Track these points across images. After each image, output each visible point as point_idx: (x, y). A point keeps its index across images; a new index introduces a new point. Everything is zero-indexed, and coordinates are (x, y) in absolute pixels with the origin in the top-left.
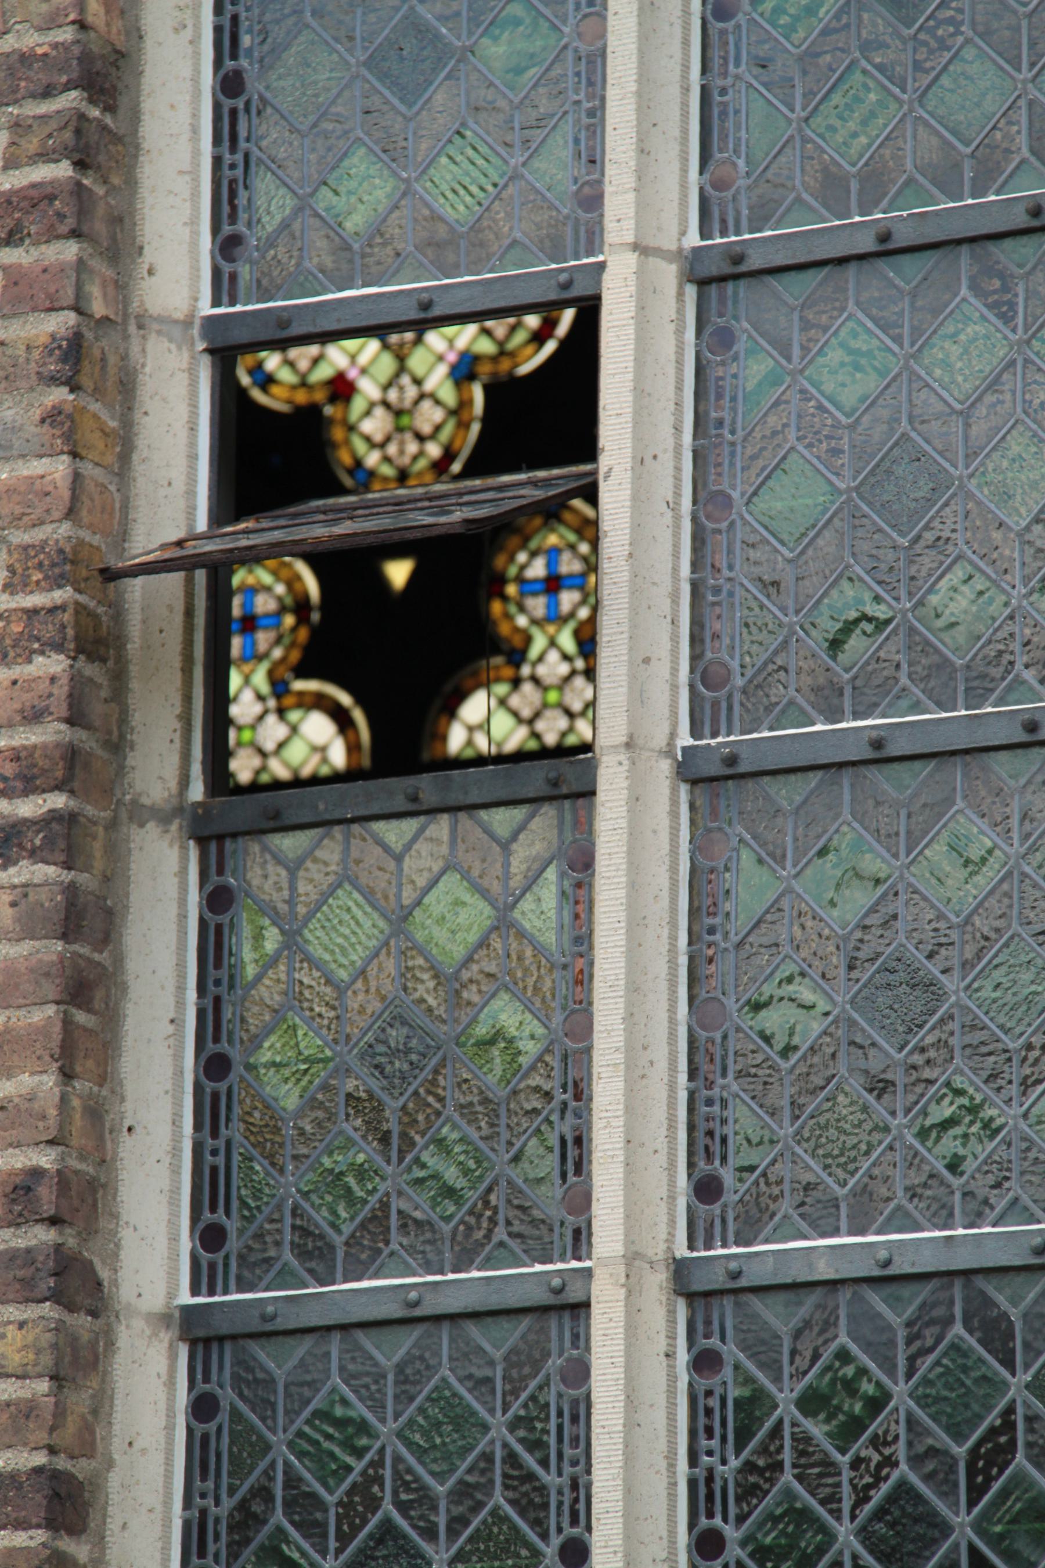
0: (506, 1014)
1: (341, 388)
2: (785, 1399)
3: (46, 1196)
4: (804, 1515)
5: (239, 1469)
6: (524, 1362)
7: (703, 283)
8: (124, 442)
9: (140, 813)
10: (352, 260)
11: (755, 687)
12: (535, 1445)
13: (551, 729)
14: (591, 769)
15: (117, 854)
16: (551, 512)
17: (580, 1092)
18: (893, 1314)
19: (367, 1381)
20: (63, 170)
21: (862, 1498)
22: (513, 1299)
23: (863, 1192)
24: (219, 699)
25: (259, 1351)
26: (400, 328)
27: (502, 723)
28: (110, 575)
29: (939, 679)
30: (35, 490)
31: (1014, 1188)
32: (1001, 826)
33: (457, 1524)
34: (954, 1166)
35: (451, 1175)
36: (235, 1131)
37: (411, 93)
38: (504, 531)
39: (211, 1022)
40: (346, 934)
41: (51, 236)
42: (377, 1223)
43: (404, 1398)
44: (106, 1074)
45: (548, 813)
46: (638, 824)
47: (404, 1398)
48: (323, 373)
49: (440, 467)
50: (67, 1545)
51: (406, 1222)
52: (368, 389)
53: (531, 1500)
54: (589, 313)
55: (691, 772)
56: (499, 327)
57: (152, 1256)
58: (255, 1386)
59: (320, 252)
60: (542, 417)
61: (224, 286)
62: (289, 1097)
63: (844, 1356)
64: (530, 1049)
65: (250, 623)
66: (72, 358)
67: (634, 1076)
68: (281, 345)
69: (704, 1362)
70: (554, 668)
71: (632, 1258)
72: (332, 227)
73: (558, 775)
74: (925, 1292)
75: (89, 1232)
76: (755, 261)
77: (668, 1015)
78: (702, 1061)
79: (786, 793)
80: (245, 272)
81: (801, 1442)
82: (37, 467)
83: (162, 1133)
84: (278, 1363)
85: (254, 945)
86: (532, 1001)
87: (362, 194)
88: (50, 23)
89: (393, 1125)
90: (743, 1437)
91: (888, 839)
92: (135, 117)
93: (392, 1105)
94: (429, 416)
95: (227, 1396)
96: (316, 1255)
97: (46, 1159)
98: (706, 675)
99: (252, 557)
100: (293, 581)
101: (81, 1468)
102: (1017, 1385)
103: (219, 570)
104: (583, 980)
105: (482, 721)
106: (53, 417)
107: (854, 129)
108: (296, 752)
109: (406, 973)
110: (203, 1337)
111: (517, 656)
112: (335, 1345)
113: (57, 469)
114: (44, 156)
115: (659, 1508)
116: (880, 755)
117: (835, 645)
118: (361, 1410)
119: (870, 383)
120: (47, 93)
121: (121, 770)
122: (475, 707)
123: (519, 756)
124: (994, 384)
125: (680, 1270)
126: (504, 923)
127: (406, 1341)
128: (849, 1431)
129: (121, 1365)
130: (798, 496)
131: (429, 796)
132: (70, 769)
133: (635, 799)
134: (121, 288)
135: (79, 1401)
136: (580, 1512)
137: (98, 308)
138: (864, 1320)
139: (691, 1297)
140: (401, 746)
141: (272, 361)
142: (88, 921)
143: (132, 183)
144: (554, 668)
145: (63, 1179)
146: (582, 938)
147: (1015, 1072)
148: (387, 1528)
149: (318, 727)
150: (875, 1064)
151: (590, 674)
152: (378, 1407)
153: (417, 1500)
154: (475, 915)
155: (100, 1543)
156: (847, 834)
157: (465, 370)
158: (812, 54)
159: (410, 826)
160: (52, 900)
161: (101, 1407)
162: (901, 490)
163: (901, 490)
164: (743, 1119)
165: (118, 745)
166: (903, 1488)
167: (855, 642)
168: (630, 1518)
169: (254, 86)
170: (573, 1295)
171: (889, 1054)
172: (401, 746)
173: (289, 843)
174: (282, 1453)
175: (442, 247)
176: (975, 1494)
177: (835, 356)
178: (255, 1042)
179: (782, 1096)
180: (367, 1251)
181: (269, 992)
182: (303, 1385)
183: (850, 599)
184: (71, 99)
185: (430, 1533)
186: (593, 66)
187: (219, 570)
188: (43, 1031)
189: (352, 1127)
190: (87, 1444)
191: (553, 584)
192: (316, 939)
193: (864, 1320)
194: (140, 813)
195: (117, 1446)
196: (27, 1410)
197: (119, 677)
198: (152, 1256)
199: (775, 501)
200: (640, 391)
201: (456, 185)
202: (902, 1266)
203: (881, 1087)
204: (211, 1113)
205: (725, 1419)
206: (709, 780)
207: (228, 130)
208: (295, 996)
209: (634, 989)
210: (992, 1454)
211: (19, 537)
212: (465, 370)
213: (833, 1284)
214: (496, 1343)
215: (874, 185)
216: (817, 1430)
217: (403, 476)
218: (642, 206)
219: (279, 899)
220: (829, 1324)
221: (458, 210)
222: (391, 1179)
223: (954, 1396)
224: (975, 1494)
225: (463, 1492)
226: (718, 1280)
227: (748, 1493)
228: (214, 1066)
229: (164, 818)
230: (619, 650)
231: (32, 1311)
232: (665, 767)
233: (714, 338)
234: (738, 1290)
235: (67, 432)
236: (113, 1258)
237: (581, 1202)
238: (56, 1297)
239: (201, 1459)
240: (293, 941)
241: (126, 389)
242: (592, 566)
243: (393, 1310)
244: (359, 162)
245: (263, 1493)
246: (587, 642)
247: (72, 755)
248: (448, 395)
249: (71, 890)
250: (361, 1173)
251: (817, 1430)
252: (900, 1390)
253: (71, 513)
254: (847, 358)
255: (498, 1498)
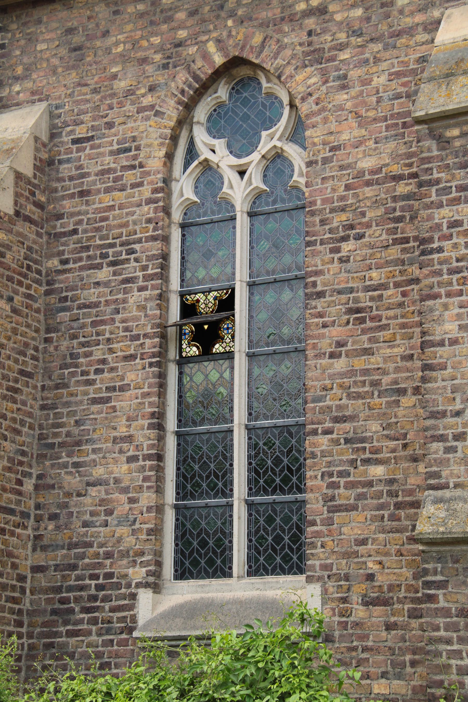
0: (222, 390)
1: (198, 301)
2: (261, 443)
3: (157, 415)
4: (263, 460)
5: (184, 453)
6: (224, 438)
7: (250, 286)
8: (167, 308)
9: (170, 361)
10: (200, 282)
11: (257, 343)
12: (226, 450)
13: (228, 349)
14: (234, 354)
15: (166, 366)
16: (228, 318)
17: (232, 400)
18: (276, 432)
19: (202, 441)
20: (159, 270)
21: (272, 457)
22: (223, 430)
23: (272, 414)
24: (181, 345)
25: (187, 437)
26: (206, 292)
27: (221, 348)
28: (166, 327)
29: (283, 342)
30: (155, 315)
31: (293, 414)
32: (292, 363)
33: (215, 461)
34: (285, 411)
35: (214, 412)
36: (183, 406)
37: (208, 259)
38: (221, 321)
39: (180, 390)
40: (199, 378)
41: (158, 279)
42: (203, 419)
43: (207, 443)
44: (165, 398)
45: (228, 361)
46: (241, 362)
47: (207, 443)
48: (195, 299)
49: (212, 312)
50: (160, 463)
51: (207, 419)
52: (202, 301)
53: (225, 458)
54: (233, 290)
55: (248, 355)
56: (220, 292)
57: (171, 423)
58: (186, 442)
59: (195, 281)
60: (227, 304)
61: (182, 286)
62: (191, 401)
63: (269, 437)
64: (225, 394)
65: (185, 334)
66: (160, 297)
67: (240, 398)
68: (189, 295)
69: (250, 438)
70: (228, 340)
71: (239, 424)
72: (197, 278)
73: (229, 356)
74: (281, 428)
75: (163, 420)
76: (257, 283)
77: (245, 390)
78: (250, 396)
79: (262, 358)
80: (185, 284)
81: (263, 449)
82: (155, 312)
83: (173, 406)
84: (189, 439)
85: (186, 380)
86: (225, 388)
87: (201, 273)
88: (158, 250)
89: (205, 405)
90: (255, 449)
91: (276, 365)
92: (169, 263)
93: (205, 402)
94: (210, 305)
95: (182, 443)
96: (195, 423)
97: (156, 410)
98: (250, 341)
99: (185, 325)
100: (191, 328)
101: (162, 453)
102: (293, 441)
103: (181, 326)
104: (233, 385)
105: (218, 348)
106: (157, 305)
107: (271, 265)
108: (191, 352)
109: (207, 384)
110: (178, 435)
111: (223, 339)
112: (197, 436)
113: (158, 312)
114: (157, 268)
115: (243, 459)
116: (275, 352)
117: (268, 337)
118: (201, 445)
119: (273, 300)
120: (157, 259)
121: (167, 355)
122: (217, 346)
123: (223, 353)
124: (291, 300)
125: (246, 426)
126: (221, 376)
127: (208, 436)
128: (270, 448)
129: (167, 439)
130: (263, 316)
131: (211, 358)
132: (160, 354)
133: (240, 359)
134: (167, 286)
135: (161, 444)
136: (232, 459)
137: (164, 289)
138: (272, 433)
139: (248, 429)
140: (206, 352)
141: (188, 297)
142: (162, 376)
143: (169, 272)
144: (228, 340)
145: (159, 413)
146: (232, 379)
147: (294, 397)
148: (205, 461)
149: (195, 349)
150: (274, 396)
151: (233, 341)
152: (203, 445)
153: (209, 458)
154: (217, 375)
155: (164, 463)
156: (270, 364)
157: (215, 298)
158: (264, 254)
159: (208, 363)
160: (157, 373)
161: (164, 444)
162: (278, 315)
163: (278, 315)
164: (255, 404)
165: (166, 351)
166: (277, 456)
167: (271, 337)
168: (239, 460)
169: (186, 258)
170: (230, 504)
171: (276, 395)
172: (206, 352)
173: (191, 365)
174: (190, 451)
175: (213, 280)
176: (287, 456)
177: (268, 296)
178: (186, 393)
179: (261, 401)
180: (202, 423)
181: (188, 386)
182: (193, 442)
183: (271, 330)
184: (161, 260)
185: (211, 462)
186: (234, 256)
187: (181, 326)
188: (156, 392)
189: (200, 405)
190: (162, 450)
191: (228, 329)
192: (194, 379)
193: (272, 433)
194: (170, 361)
195: (167, 450)
196: (154, 445)
197: (167, 342)
198: (171, 423)
199: (259, 317)
200: (241, 301)
201: (215, 272)
202: (278, 425)
203: (275, 400)
204: (180, 403)
205: (253, 446)
206: (251, 356)
207: (182, 264)
208: (192, 387)
209: (240, 386)
210: (290, 451)
211: (153, 322)
212: (215, 298)
213: (268, 428)
214: (220, 436)
215: (274, 272)
216: (265, 448)
217: (207, 313)
218: (241, 275)
219: (189, 373)
220: (267, 433)
221: (215, 276)
222: (205, 413)
223: (285, 443)
224: (287, 456)
225: (215, 457)
226: (252, 427)
227: (256, 457)
228: (180, 397)
229: (173, 361)
230: (238, 339)
231: (154, 431)
232: (244, 354)
233: (251, 294)
234: (254, 428)
235: (159, 307)
236: (166, 424)
237: (232, 416)
238: (158, 429)
239: (178, 452)
240: (191, 379)
241: (168, 301)
242: (234, 326)
243: (206, 431)
244: (201, 269)
245: (187, 457)
246: (233, 337)
247: (160, 352)
248: (213, 302)
249: (160, 372)
250: (201, 412)
251: (265, 448)
252: (277, 442)
253: (160, 318)
254: (270, 297)
255: (220, 458)
